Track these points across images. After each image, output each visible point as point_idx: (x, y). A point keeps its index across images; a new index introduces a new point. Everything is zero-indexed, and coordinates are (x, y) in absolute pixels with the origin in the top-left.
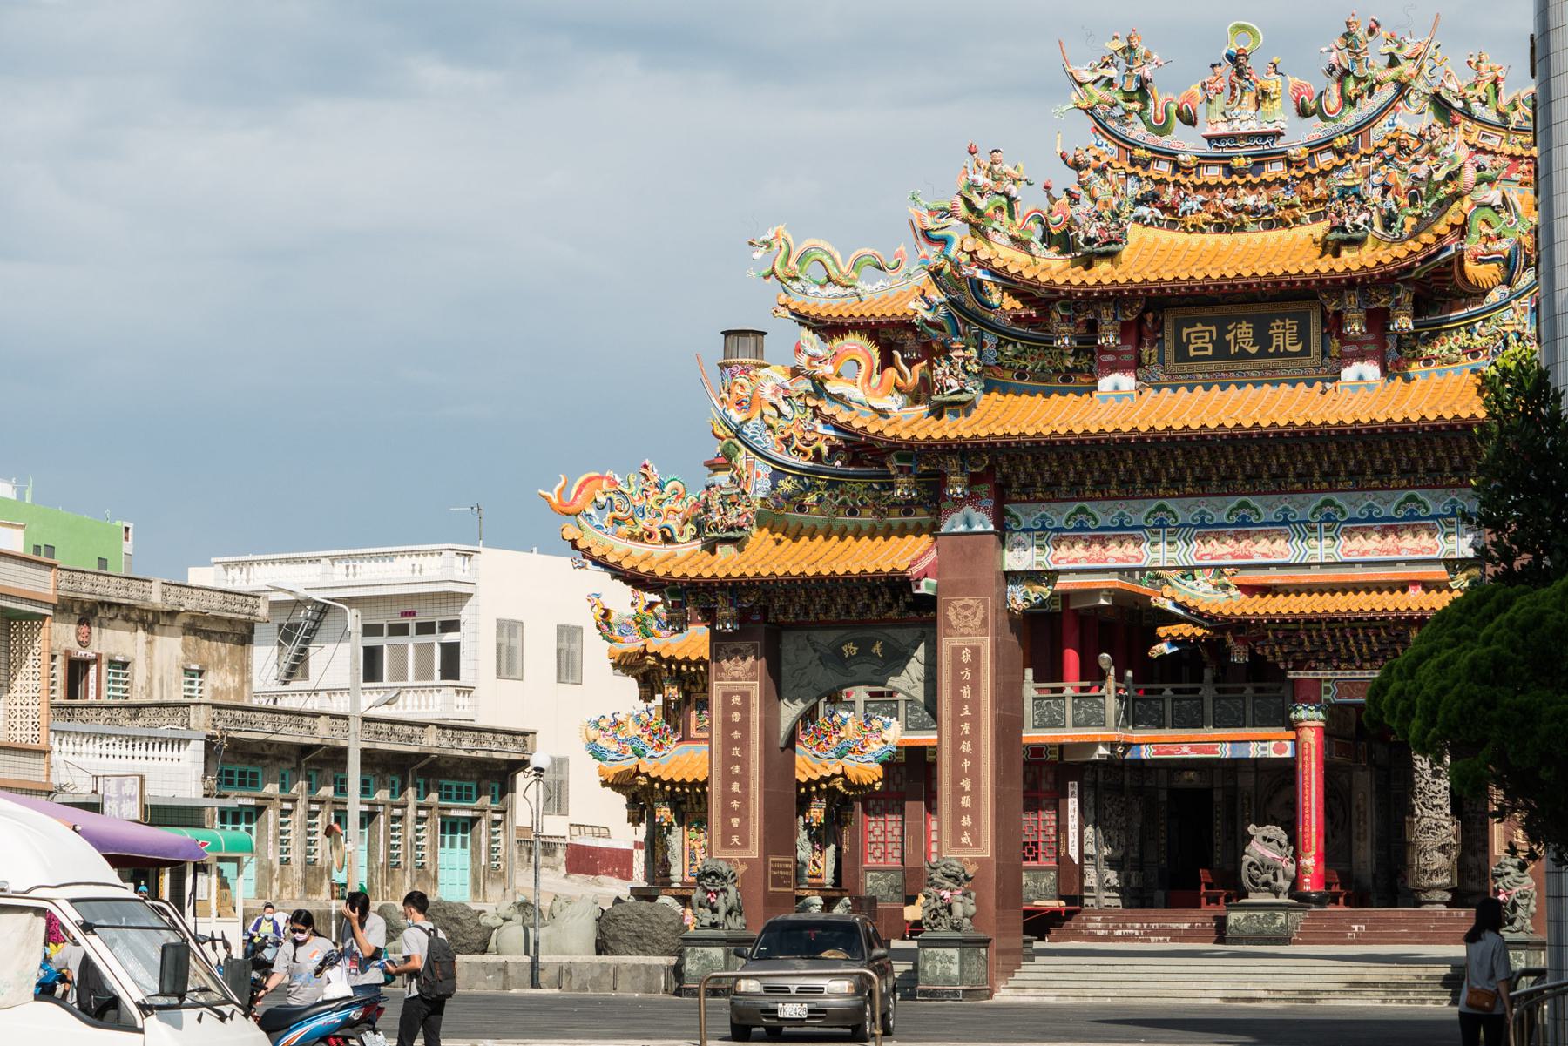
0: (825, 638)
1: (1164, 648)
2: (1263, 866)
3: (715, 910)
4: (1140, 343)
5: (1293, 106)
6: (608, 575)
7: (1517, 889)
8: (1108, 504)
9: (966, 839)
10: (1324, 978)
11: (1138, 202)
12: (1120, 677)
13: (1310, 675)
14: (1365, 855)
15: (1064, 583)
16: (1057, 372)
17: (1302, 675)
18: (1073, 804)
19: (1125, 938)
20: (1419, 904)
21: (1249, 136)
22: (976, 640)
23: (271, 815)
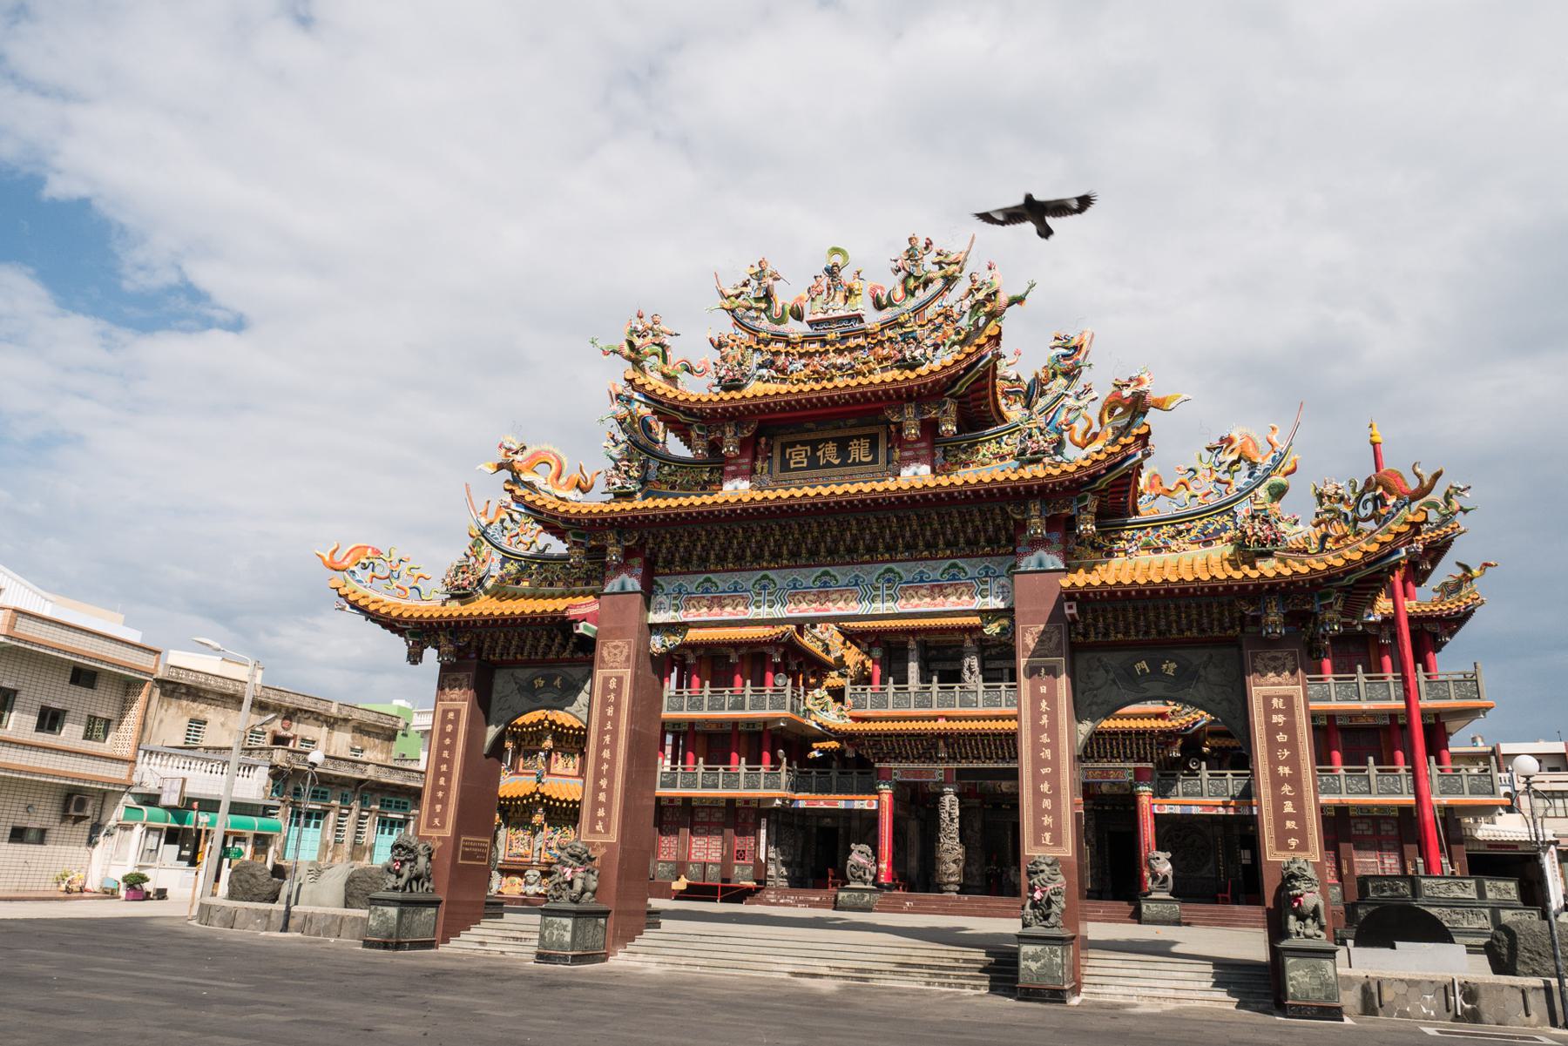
0: (523, 674)
1: (816, 754)
2: (858, 867)
3: (399, 876)
4: (755, 459)
5: (870, 301)
6: (378, 627)
7: (1051, 886)
8: (726, 575)
9: (599, 827)
10: (877, 958)
11: (760, 366)
12: (789, 764)
14: (913, 863)
15: (693, 635)
16: (697, 484)
18: (763, 832)
19: (785, 904)
20: (942, 891)
21: (839, 320)
22: (620, 672)
23: (332, 816)
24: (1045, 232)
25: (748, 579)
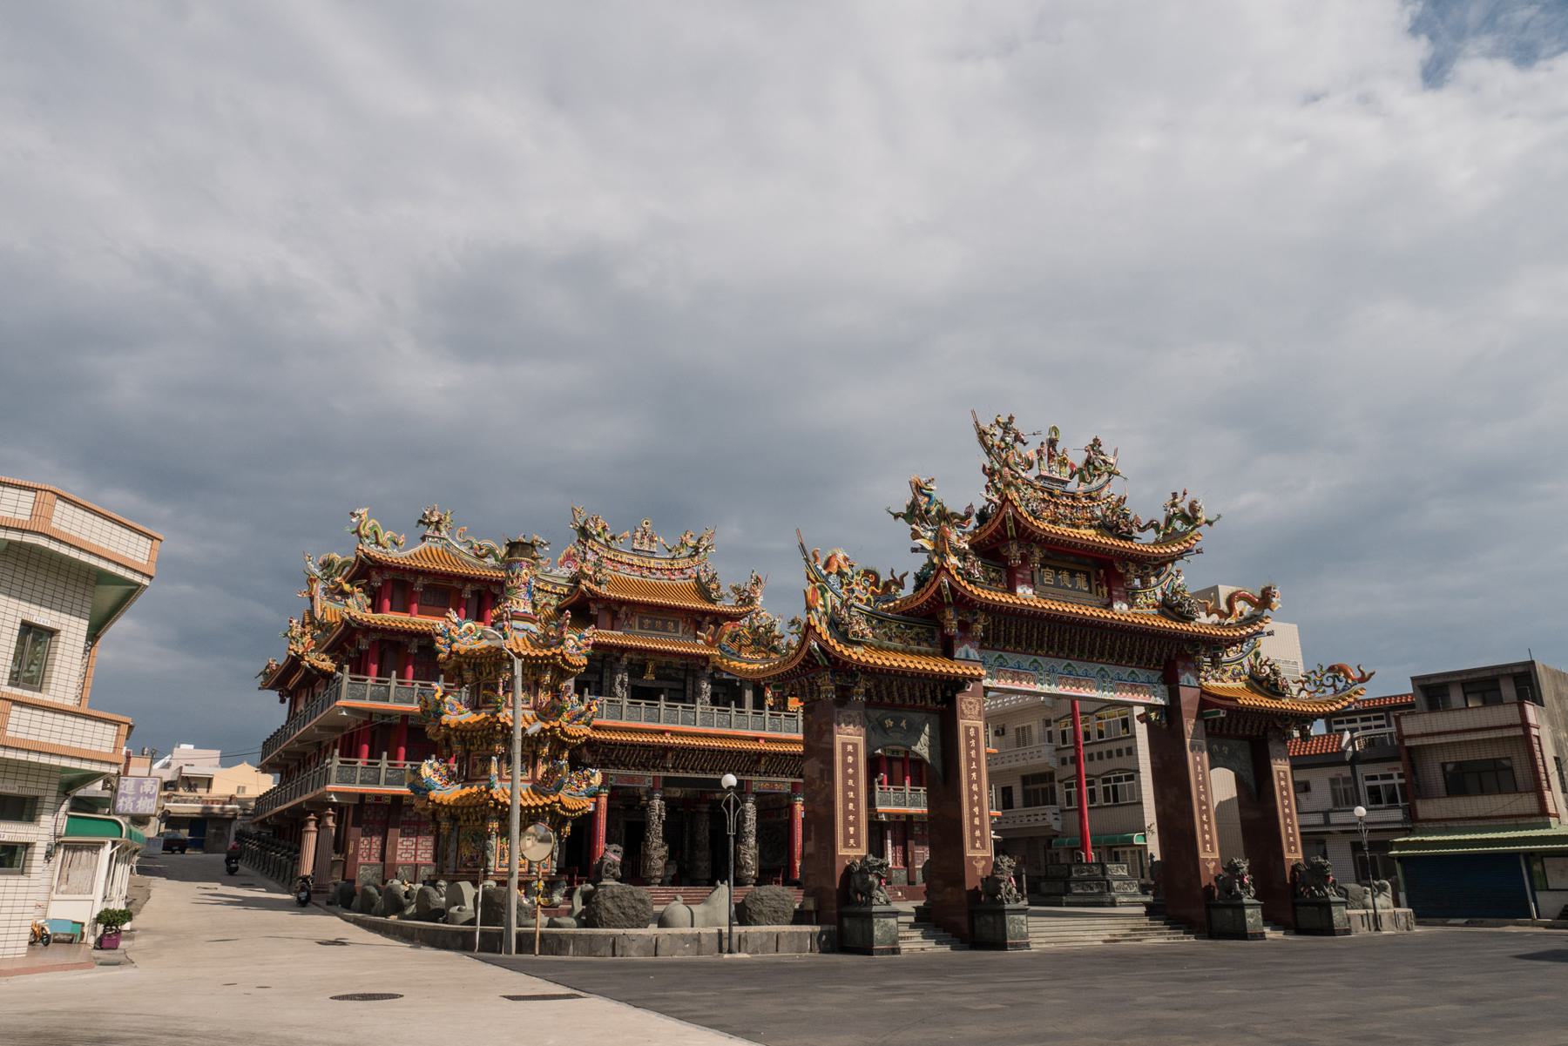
24: (1011, 418)
25: (1026, 660)
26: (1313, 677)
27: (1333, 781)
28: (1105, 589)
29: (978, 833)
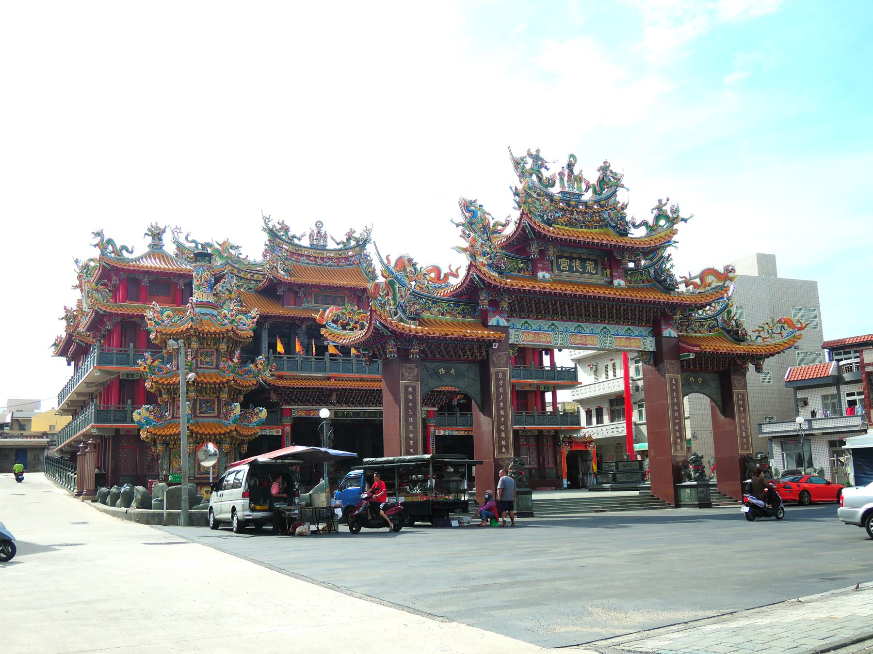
13: (287, 407)
17: (287, 407)
26: (766, 327)
27: (824, 397)
28: (608, 271)
29: (503, 443)
